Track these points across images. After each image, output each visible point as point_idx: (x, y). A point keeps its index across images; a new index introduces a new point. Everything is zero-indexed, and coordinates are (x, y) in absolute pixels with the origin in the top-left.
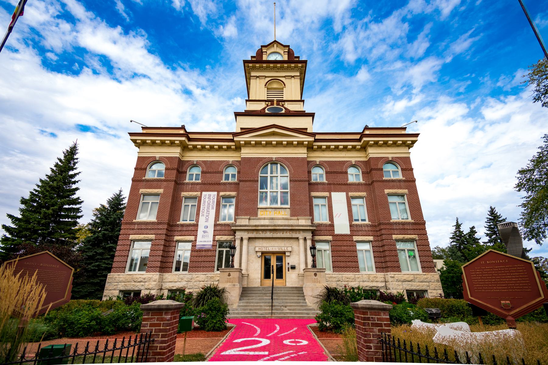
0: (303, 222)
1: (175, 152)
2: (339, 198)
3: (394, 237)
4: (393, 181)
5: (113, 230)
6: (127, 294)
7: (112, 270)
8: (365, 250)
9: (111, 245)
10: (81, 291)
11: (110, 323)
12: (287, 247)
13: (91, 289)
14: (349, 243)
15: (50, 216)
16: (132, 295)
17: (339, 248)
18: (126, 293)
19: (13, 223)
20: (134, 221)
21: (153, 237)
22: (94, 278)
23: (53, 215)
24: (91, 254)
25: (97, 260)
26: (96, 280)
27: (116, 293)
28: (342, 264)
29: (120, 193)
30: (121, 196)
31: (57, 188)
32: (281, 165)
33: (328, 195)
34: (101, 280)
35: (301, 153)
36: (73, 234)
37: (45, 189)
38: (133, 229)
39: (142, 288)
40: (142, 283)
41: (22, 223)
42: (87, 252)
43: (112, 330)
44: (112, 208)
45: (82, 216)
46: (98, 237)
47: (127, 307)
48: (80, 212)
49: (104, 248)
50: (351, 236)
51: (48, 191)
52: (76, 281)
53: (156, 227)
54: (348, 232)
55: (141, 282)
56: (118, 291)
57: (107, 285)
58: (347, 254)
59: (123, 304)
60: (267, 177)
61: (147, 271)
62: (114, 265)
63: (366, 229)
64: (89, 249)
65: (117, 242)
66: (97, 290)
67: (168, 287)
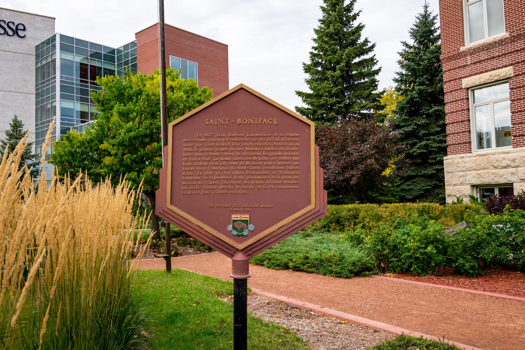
5: (431, 82)
6: (487, 190)
7: (449, 149)
9: (437, 108)
10: (412, 189)
11: (464, 251)
13: (422, 185)
15: (340, 80)
16: (497, 192)
18: (486, 190)
19: (304, 101)
20: (462, 49)
21: (509, 71)
22: (426, 167)
23: (342, 77)
24: (410, 129)
25: (421, 139)
26: (430, 171)
27: (467, 190)
29: (426, 11)
30: (429, 15)
31: (336, 34)
34: (438, 171)
36: (375, 101)
37: (323, 41)
38: (464, 66)
39: (512, 179)
40: (511, 170)
41: (314, 100)
42: (403, 126)
43: (473, 267)
44: (420, 43)
45: (380, 70)
46: (412, 99)
47: (493, 218)
48: (375, 63)
49: (428, 116)
51: (326, 43)
52: (39, 65)
53: (510, 48)
55: (507, 167)
56: (469, 187)
57: (447, 177)
59: (482, 211)
61: (516, 145)
62: (450, 140)
64: (405, 120)
65: (443, 100)
66: (436, 187)
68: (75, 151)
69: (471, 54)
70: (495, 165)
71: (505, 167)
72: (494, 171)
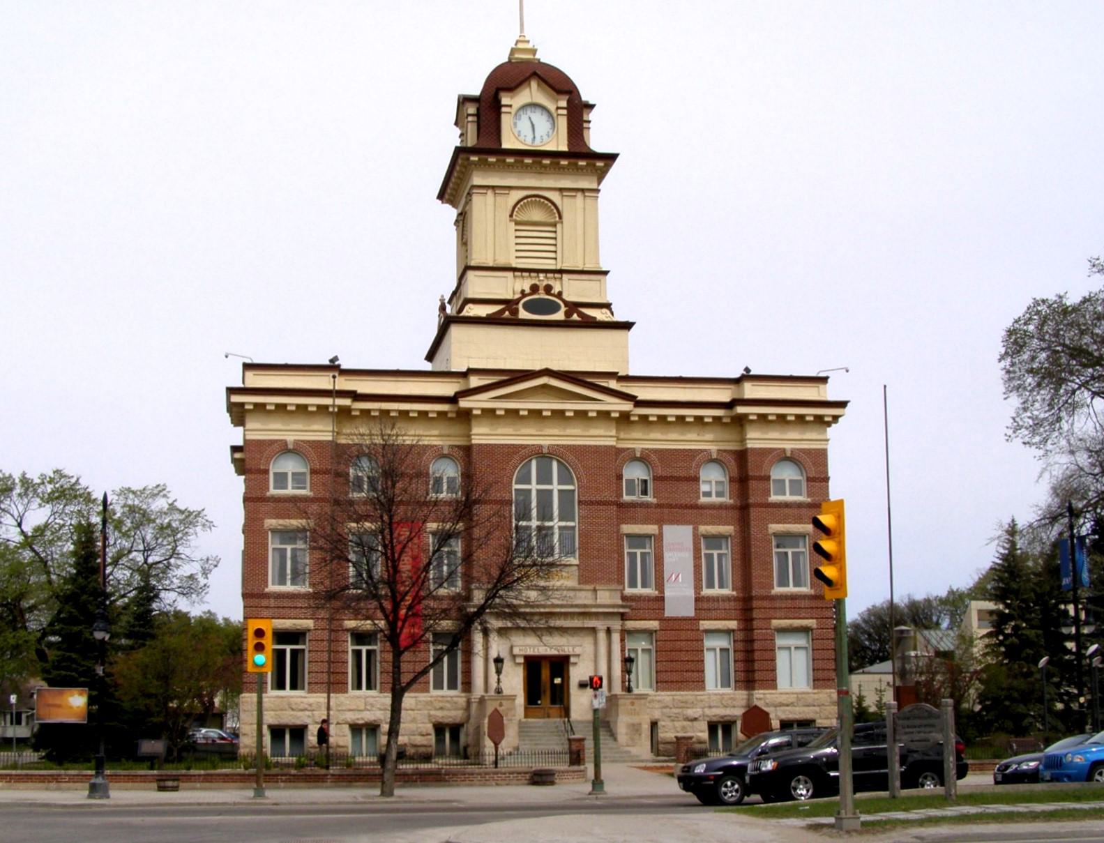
0: (607, 597)
1: (321, 431)
2: (678, 541)
3: (775, 623)
4: (787, 505)
8: (714, 655)
12: (574, 646)
14: (690, 635)
17: (669, 645)
28: (675, 677)
32: (558, 461)
33: (657, 532)
35: (603, 437)
40: (307, 713)
50: (696, 619)
54: (690, 612)
55: (306, 710)
58: (684, 657)
60: (530, 491)
63: (727, 605)
67: (349, 720)
68: (153, 678)
69: (275, 598)
70: (294, 707)
71: (302, 710)
72: (292, 713)
